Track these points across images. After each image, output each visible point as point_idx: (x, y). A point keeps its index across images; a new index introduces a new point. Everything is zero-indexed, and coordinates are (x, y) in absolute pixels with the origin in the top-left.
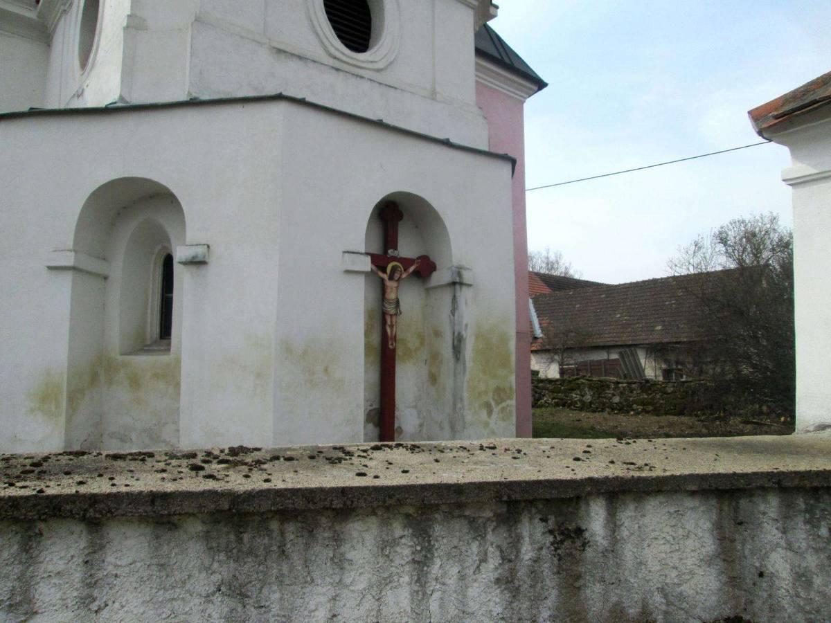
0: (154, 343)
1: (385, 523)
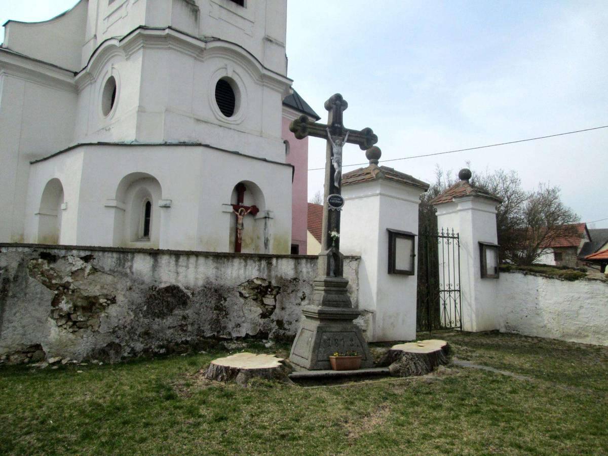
0: (142, 238)
1: (240, 260)
